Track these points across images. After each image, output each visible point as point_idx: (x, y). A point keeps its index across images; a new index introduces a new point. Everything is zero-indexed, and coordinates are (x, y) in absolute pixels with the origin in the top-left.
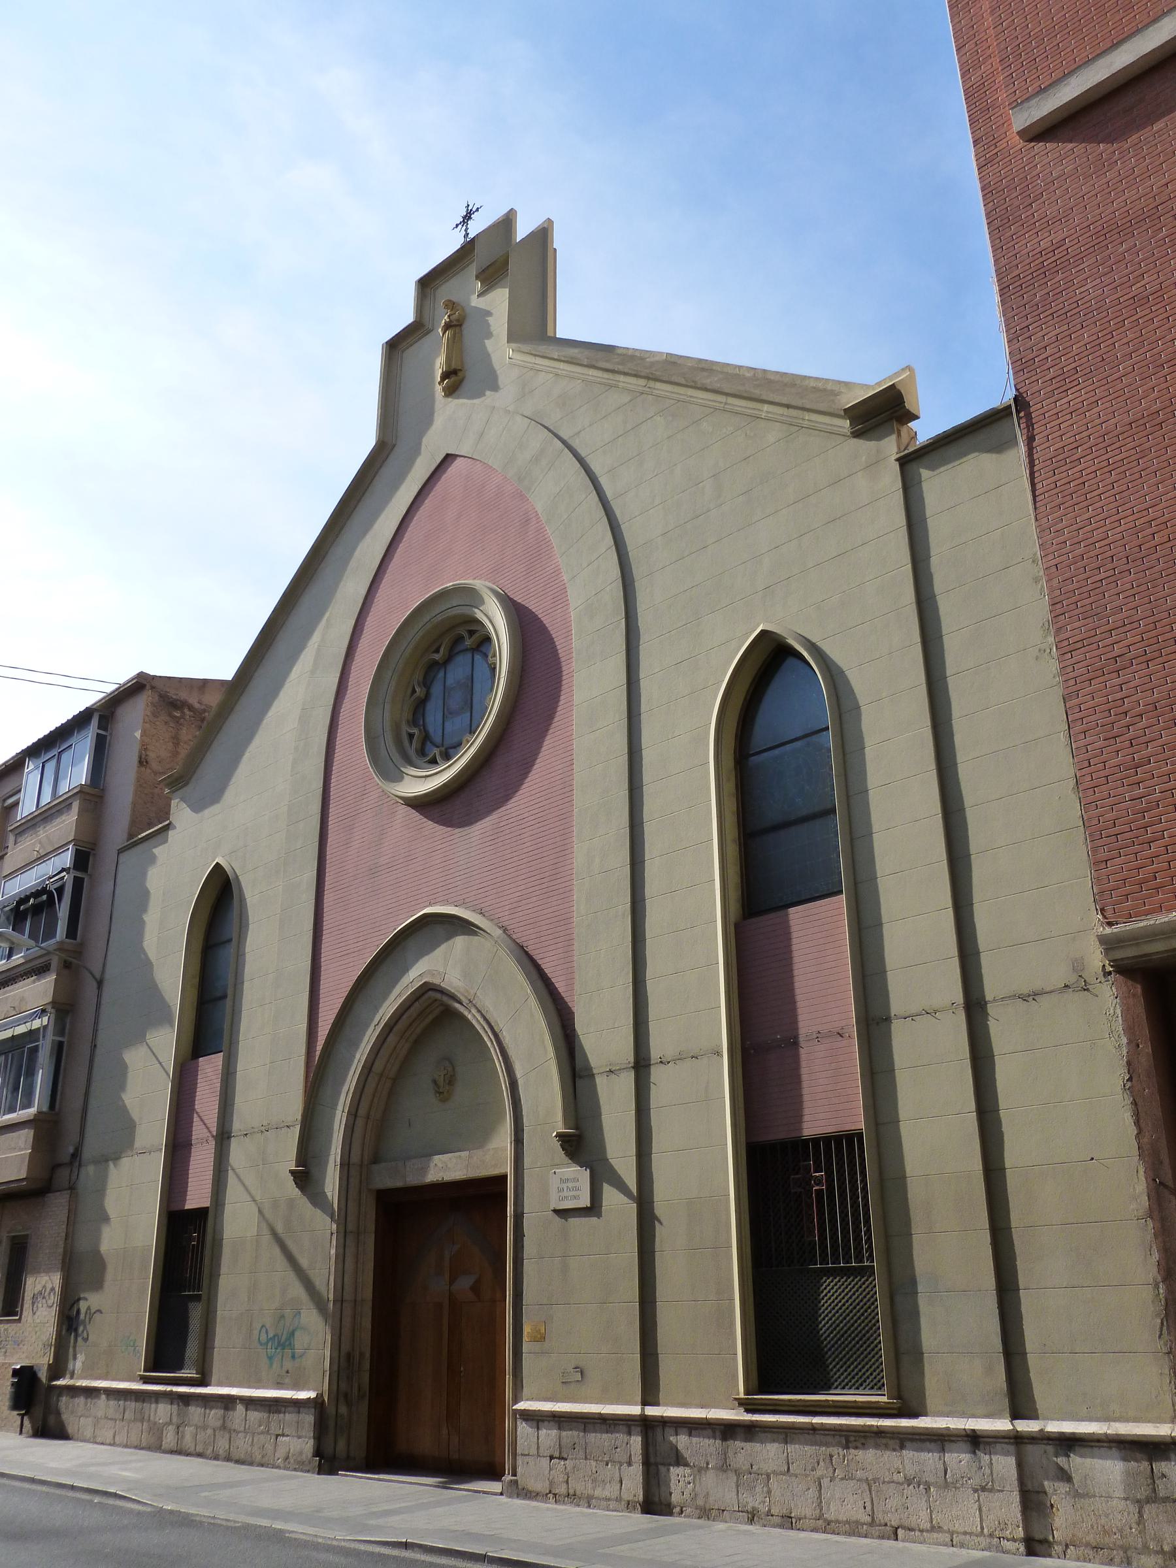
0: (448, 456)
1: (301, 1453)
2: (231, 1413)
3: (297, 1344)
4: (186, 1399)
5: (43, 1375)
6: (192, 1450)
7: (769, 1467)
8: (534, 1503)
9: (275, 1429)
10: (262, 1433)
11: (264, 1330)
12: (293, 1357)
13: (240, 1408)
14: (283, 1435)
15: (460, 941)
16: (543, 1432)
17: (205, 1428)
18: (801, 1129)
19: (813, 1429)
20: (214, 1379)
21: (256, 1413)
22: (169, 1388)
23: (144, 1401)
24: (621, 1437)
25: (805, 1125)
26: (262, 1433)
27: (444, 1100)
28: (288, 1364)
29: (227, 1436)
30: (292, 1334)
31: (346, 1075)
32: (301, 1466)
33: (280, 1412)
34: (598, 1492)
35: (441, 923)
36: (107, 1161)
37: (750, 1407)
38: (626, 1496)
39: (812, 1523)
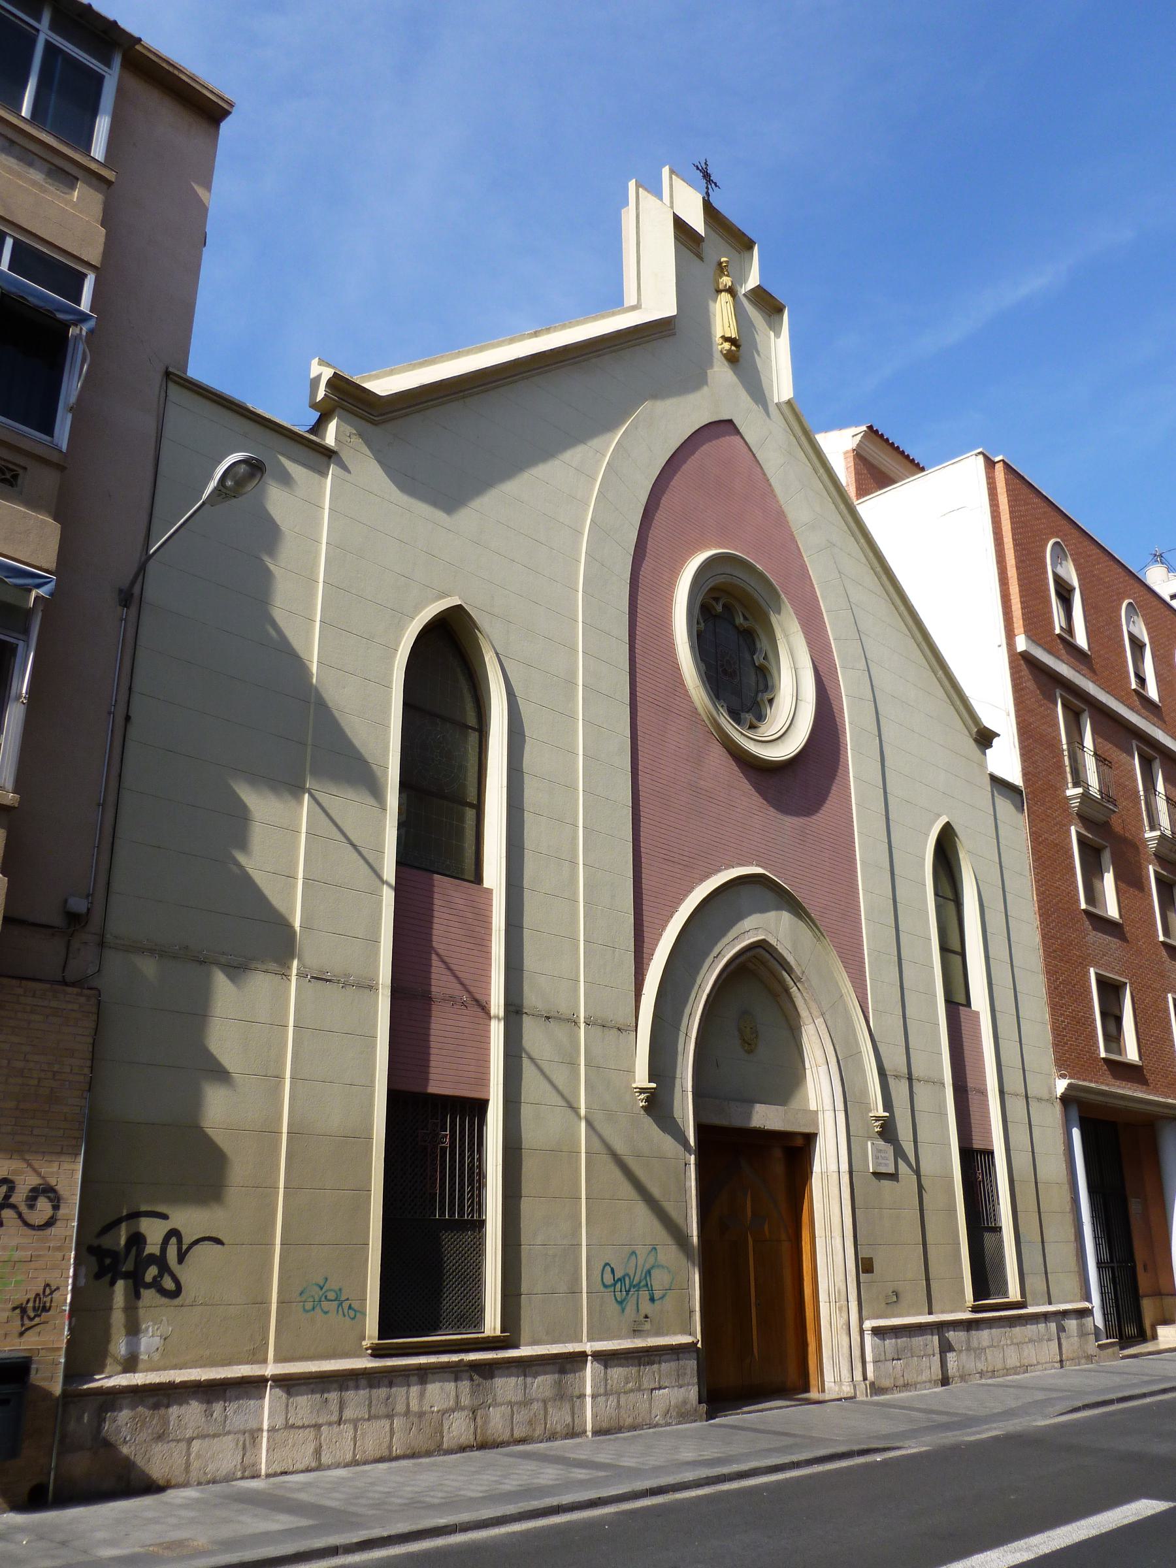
0: (730, 421)
1: (685, 1402)
2: (570, 1376)
3: (656, 1285)
4: (486, 1370)
5: (51, 1379)
6: (506, 1436)
7: (985, 1343)
8: (432, 1459)
9: (646, 1384)
10: (632, 1391)
11: (608, 1269)
12: (652, 1300)
13: (590, 1370)
14: (660, 1388)
15: (786, 917)
16: (887, 1342)
17: (526, 1403)
18: (426, 1086)
19: (1000, 1318)
20: (141, 1366)
21: (621, 1369)
22: (455, 1358)
23: (391, 1385)
24: (1042, 1326)
25: (431, 1083)
26: (632, 1391)
27: (750, 1052)
28: (646, 1307)
29: (567, 1406)
30: (649, 1272)
31: (689, 995)
32: (684, 1416)
33: (653, 1364)
34: (920, 1379)
35: (772, 889)
36: (203, 962)
37: (975, 1309)
38: (934, 1378)
39: (1001, 1372)
